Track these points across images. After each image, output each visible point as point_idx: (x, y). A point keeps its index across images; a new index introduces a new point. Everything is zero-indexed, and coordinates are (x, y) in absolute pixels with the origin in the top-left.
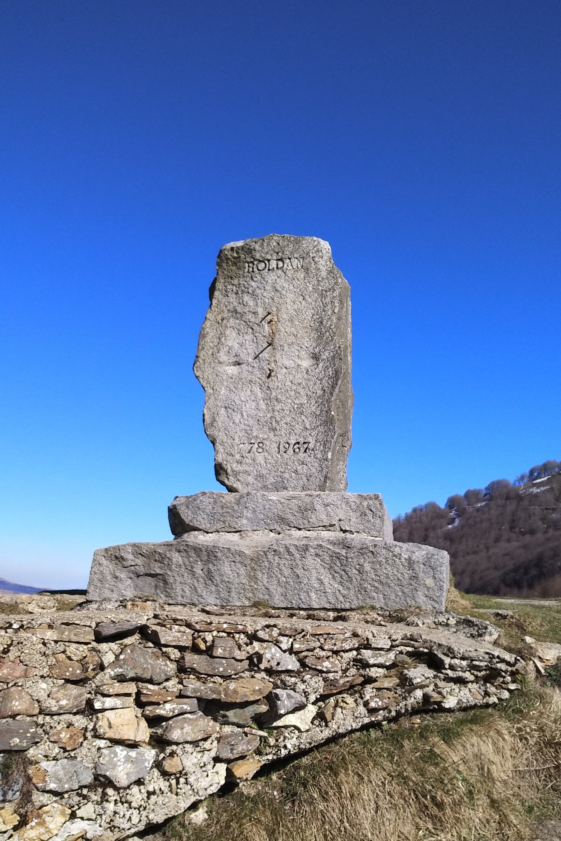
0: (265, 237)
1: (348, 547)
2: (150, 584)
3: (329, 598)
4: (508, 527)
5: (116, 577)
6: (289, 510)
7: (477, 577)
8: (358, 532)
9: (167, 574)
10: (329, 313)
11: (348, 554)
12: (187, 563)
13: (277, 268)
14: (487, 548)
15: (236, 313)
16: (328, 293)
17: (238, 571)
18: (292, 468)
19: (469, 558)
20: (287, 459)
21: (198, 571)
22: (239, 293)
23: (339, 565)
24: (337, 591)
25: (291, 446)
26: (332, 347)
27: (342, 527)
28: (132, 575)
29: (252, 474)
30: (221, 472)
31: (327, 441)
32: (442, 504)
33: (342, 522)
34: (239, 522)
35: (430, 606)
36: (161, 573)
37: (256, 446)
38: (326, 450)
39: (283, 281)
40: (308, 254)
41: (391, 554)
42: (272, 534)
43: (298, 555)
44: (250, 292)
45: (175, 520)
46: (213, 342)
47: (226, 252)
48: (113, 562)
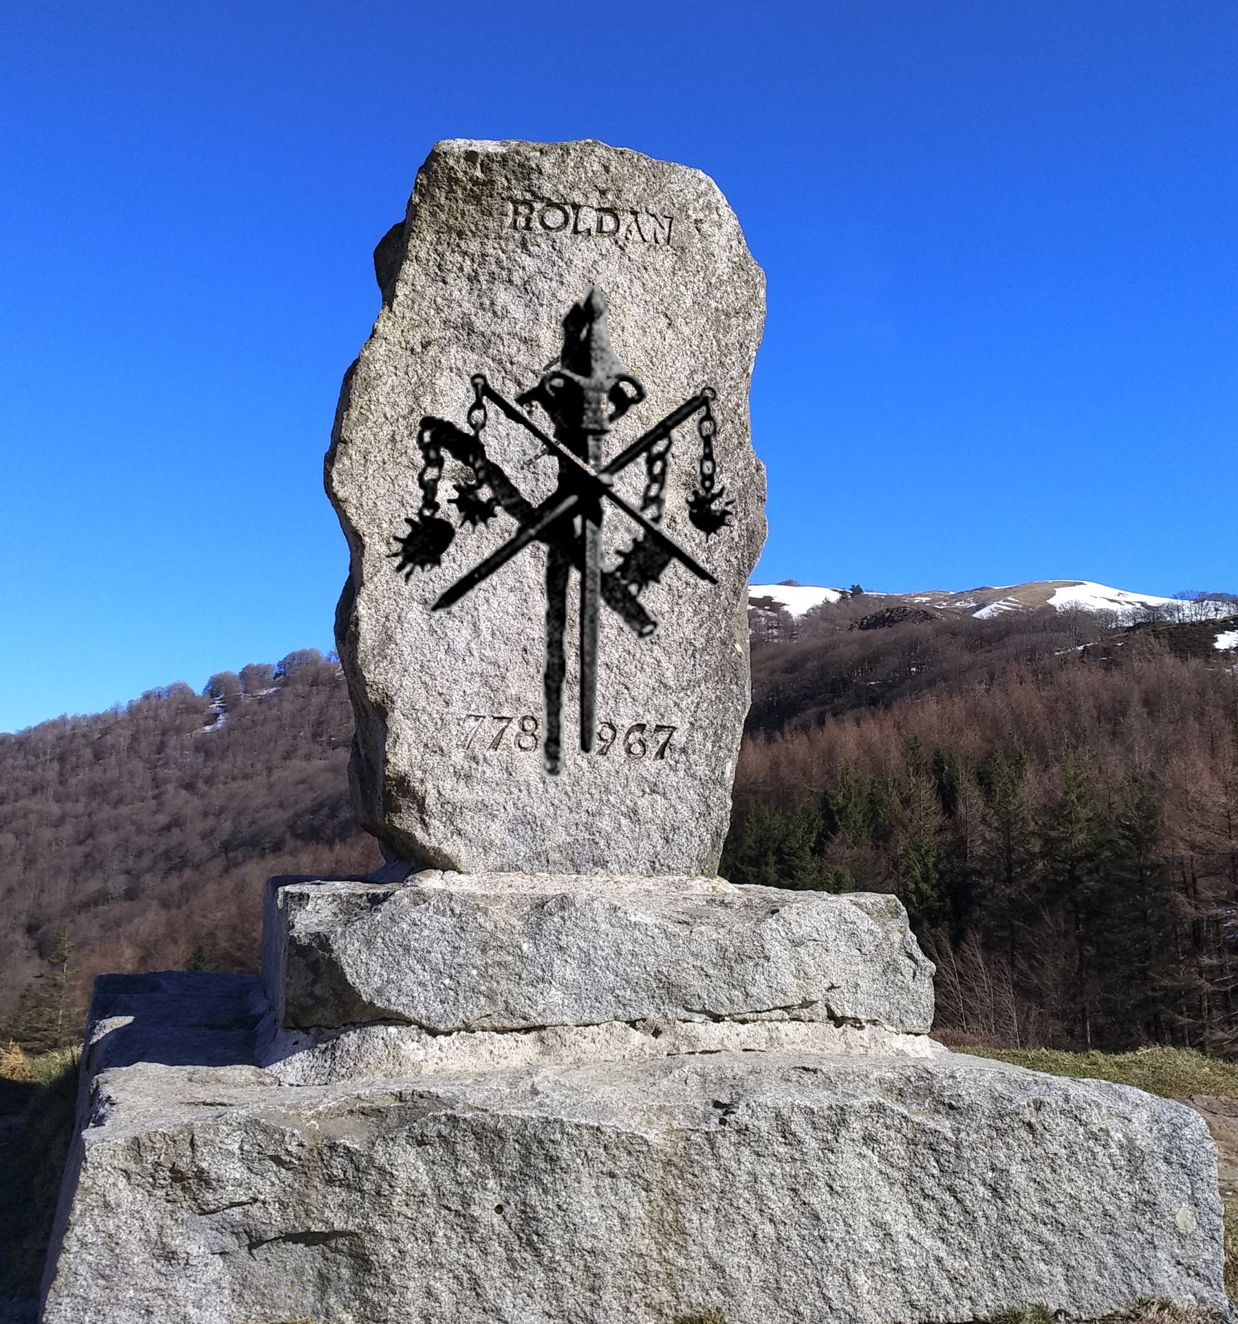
0: (571, 145)
1: (951, 1107)
2: (299, 1273)
3: (909, 1287)
4: (309, 735)
5: (170, 1256)
6: (691, 959)
7: (245, 821)
8: (874, 1022)
9: (370, 1231)
10: (734, 373)
11: (963, 1135)
12: (449, 1186)
13: (600, 230)
14: (270, 770)
15: (471, 331)
16: (733, 321)
17: (622, 1207)
18: (623, 802)
19: (235, 785)
20: (609, 774)
21: (484, 1212)
22: (482, 278)
23: (936, 1172)
24: (932, 1264)
25: (621, 735)
26: (741, 464)
27: (833, 1007)
28: (230, 1242)
29: (502, 815)
30: (403, 802)
31: (724, 727)
32: (198, 687)
33: (835, 994)
34: (539, 998)
35: (1190, 1296)
36: (351, 1228)
37: (515, 727)
38: (721, 754)
39: (614, 267)
40: (683, 208)
41: (1081, 1130)
42: (637, 1037)
43: (814, 1144)
44: (516, 278)
45: (314, 982)
46: (395, 405)
47: (451, 162)
48: (160, 1193)
